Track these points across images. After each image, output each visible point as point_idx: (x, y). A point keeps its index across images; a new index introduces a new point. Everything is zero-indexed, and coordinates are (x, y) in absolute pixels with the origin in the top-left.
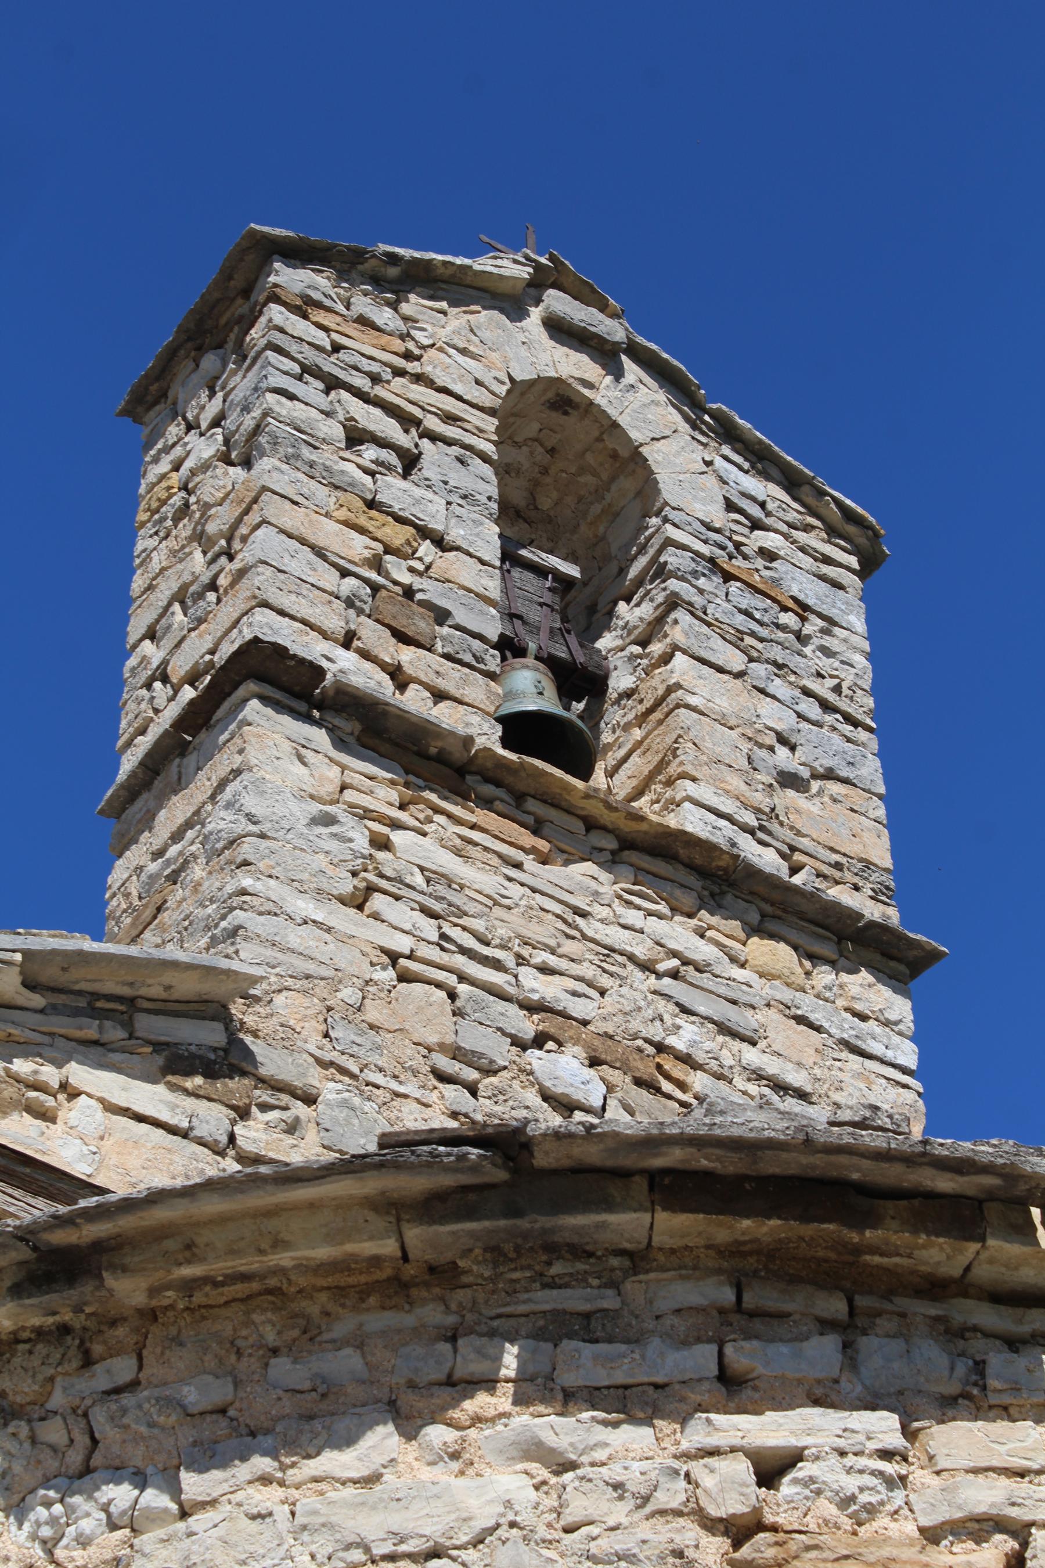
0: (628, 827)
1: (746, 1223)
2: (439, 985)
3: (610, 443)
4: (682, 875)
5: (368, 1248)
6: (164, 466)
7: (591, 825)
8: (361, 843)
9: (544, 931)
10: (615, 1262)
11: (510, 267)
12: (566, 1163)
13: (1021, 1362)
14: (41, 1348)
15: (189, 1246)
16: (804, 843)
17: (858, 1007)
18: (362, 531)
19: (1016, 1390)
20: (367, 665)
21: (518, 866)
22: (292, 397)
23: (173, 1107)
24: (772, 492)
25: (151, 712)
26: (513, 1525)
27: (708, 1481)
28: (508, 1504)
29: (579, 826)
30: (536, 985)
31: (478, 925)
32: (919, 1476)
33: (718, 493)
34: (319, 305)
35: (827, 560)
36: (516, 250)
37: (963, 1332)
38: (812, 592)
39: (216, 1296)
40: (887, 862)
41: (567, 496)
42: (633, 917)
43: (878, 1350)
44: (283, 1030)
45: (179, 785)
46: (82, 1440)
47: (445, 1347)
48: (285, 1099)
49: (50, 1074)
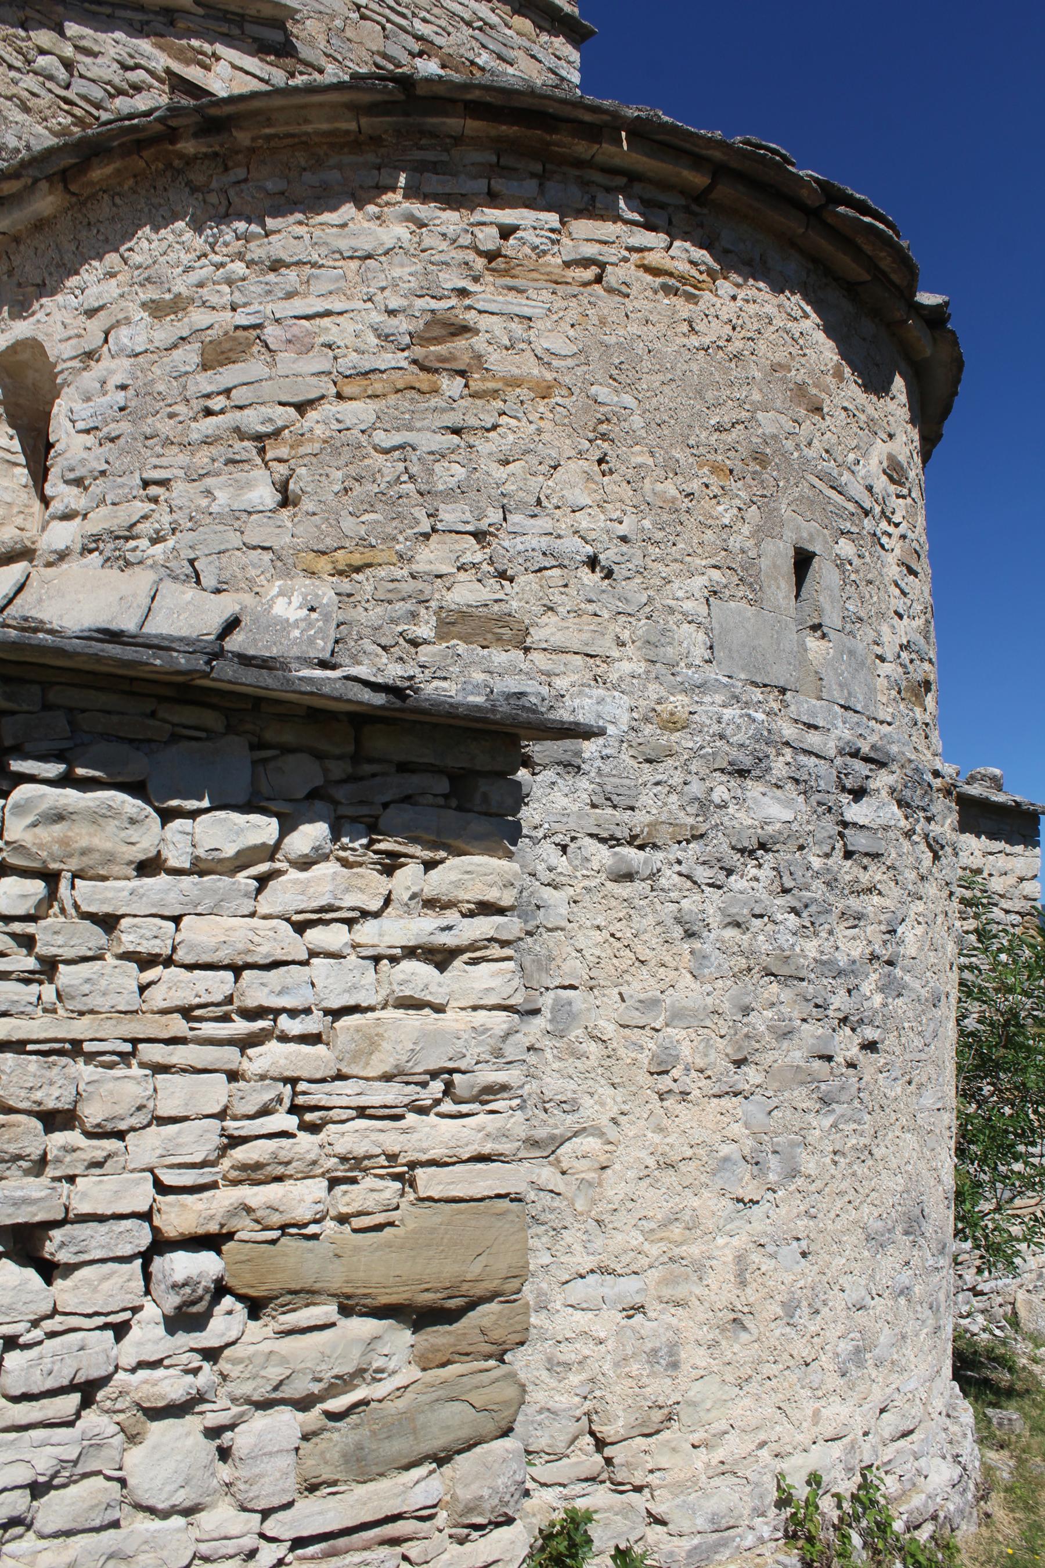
1: (504, 128)
2: (378, 23)
5: (344, 126)
10: (448, 141)
14: (206, 162)
15: (268, 119)
19: (607, 209)
23: (262, 69)
27: (480, 236)
28: (399, 239)
30: (420, 28)
32: (565, 240)
44: (310, 34)
46: (225, 203)
47: (376, 172)
48: (310, 70)
49: (207, 47)
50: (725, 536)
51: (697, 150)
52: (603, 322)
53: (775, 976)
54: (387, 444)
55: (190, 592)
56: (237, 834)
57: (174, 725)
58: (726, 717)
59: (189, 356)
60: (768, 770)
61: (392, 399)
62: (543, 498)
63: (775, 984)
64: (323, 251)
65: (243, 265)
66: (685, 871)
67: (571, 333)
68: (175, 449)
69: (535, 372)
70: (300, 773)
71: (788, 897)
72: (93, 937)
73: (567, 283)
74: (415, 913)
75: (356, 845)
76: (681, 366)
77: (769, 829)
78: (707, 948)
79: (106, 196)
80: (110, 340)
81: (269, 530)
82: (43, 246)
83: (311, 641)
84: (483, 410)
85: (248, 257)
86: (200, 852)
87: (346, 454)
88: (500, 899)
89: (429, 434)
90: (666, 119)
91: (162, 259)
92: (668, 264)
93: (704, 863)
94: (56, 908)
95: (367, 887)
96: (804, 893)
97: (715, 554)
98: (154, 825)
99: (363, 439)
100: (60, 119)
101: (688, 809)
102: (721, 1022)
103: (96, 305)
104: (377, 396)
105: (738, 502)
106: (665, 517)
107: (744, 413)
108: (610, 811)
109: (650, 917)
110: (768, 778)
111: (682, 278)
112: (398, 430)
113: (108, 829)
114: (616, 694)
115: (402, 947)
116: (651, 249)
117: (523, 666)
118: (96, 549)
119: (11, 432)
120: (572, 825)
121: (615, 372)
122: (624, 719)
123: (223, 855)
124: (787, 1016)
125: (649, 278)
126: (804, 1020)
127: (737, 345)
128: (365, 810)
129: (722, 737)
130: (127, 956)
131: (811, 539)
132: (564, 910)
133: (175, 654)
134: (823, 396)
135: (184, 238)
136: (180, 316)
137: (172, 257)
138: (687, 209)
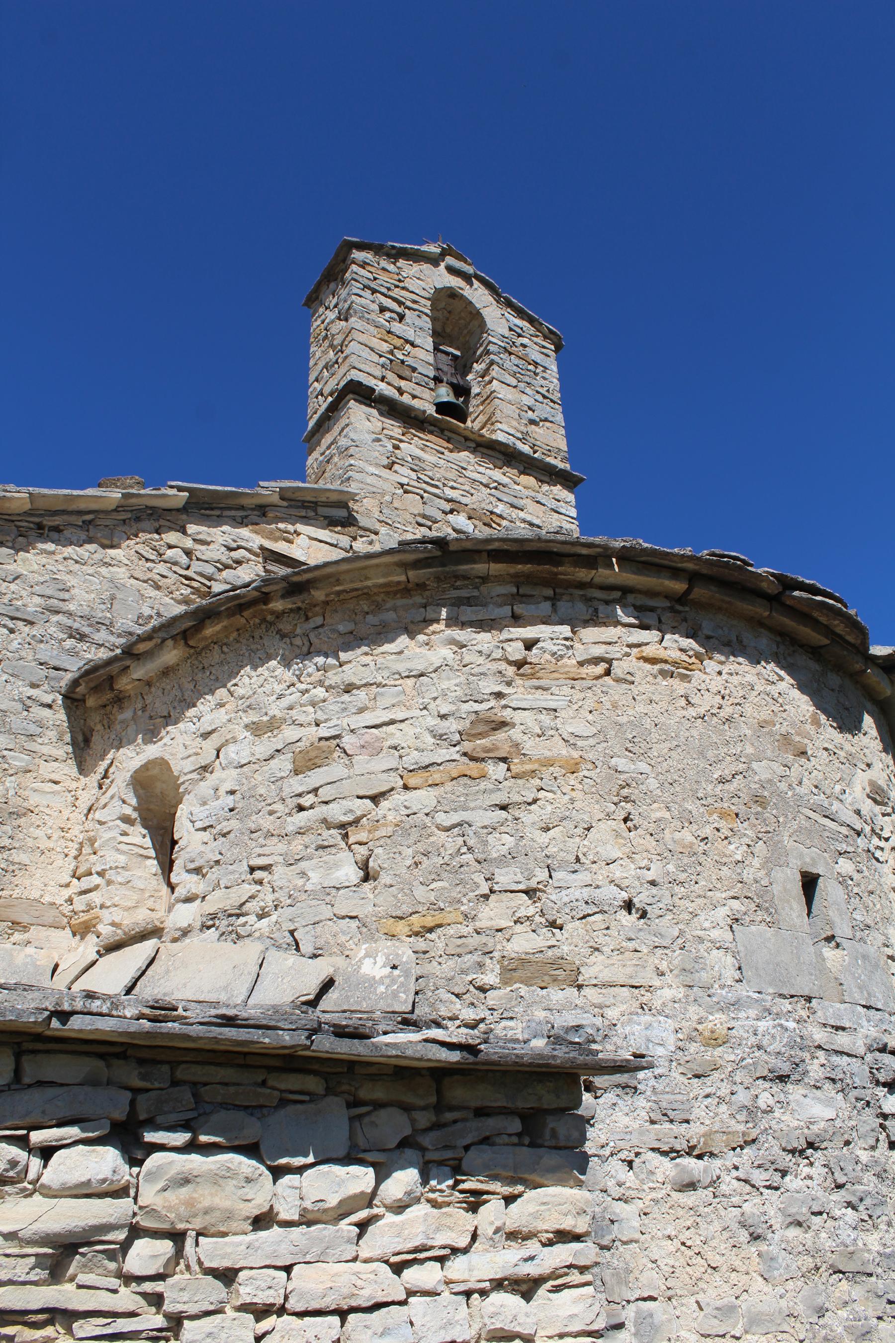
0: (479, 439)
1: (520, 566)
2: (417, 494)
3: (469, 309)
4: (497, 455)
5: (396, 579)
6: (319, 322)
7: (467, 439)
8: (390, 448)
9: (452, 475)
10: (477, 580)
11: (433, 249)
12: (460, 548)
13: (610, 608)
14: (292, 615)
15: (338, 580)
16: (538, 443)
17: (557, 497)
18: (386, 341)
19: (608, 617)
20: (390, 387)
21: (443, 453)
22: (361, 296)
23: (331, 537)
24: (525, 324)
25: (318, 406)
26: (446, 665)
27: (509, 649)
28: (445, 659)
29: (463, 440)
31: (430, 473)
32: (577, 645)
33: (506, 325)
34: (369, 264)
35: (544, 347)
36: (435, 243)
37: (591, 599)
38: (539, 358)
39: (347, 596)
40: (566, 449)
41: (455, 327)
42: (481, 469)
43: (564, 606)
44: (366, 510)
45: (328, 430)
46: (307, 644)
48: (368, 533)
49: (291, 528)
50: (739, 871)
51: (674, 564)
52: (615, 706)
53: (844, 1273)
54: (447, 824)
55: (291, 959)
56: (339, 1184)
57: (282, 1091)
58: (764, 1030)
59: (283, 764)
60: (806, 1073)
61: (449, 786)
62: (581, 856)
63: (844, 1281)
64: (386, 674)
65: (323, 690)
66: (742, 1176)
67: (590, 717)
68: (275, 840)
69: (564, 752)
70: (391, 1125)
71: (843, 1192)
72: (215, 1290)
73: (583, 679)
74: (500, 1245)
75: (443, 1186)
76: (684, 734)
77: (815, 1128)
78: (774, 1249)
79: (216, 646)
80: (221, 755)
81: (355, 902)
82: (168, 687)
83: (395, 995)
84: (524, 788)
85: (327, 684)
86: (308, 1204)
87: (415, 834)
88: (575, 1226)
89: (481, 812)
90: (646, 545)
91: (260, 690)
92: (662, 654)
93: (759, 1166)
94: (182, 1266)
95: (455, 1226)
96: (857, 1187)
97: (732, 887)
98: (266, 1183)
99: (427, 820)
100: (182, 591)
101: (738, 1116)
102: (798, 1325)
103: (210, 729)
104: (437, 785)
105: (746, 840)
106: (686, 860)
107: (741, 765)
108: (667, 1125)
109: (716, 1223)
110: (806, 1080)
111: (675, 664)
112: (455, 810)
113: (227, 1188)
114: (661, 1018)
115: (490, 1280)
116: (647, 644)
117: (578, 1002)
118: (213, 926)
119: (145, 831)
120: (635, 1142)
121: (629, 745)
122: (671, 1041)
123: (327, 1205)
124: (862, 1315)
125: (648, 666)
126: (880, 1318)
127: (727, 711)
128: (449, 1154)
129: (759, 1048)
130: (244, 1308)
131: (814, 862)
132: (636, 1223)
133: (281, 1032)
134: (806, 741)
135: (276, 673)
136: (275, 733)
137: (267, 688)
138: (672, 609)
